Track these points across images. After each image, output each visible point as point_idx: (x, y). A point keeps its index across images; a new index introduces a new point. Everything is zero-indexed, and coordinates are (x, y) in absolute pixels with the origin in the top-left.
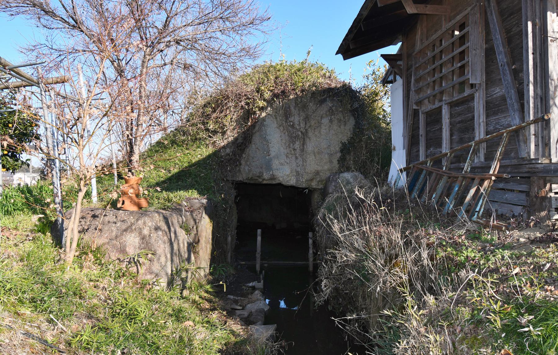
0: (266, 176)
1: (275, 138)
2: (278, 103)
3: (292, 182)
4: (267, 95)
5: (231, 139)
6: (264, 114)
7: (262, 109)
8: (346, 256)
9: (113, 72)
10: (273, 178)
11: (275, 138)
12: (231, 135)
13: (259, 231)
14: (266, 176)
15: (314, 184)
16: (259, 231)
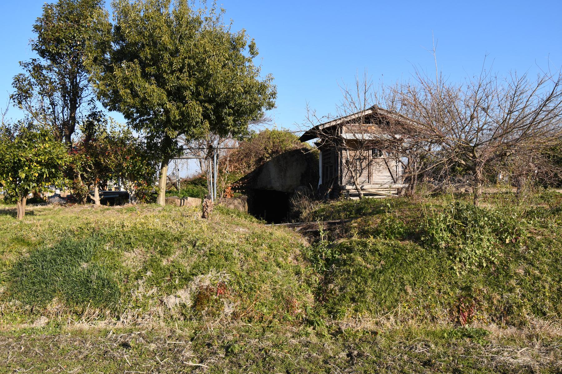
0: (269, 187)
1: (273, 172)
2: (274, 156)
3: (280, 189)
4: (270, 151)
5: (252, 170)
6: (268, 160)
7: (267, 158)
8: (296, 209)
9: (371, 190)
10: (272, 188)
11: (273, 172)
12: (253, 169)
13: (265, 211)
14: (269, 187)
15: (290, 191)
16: (265, 211)
